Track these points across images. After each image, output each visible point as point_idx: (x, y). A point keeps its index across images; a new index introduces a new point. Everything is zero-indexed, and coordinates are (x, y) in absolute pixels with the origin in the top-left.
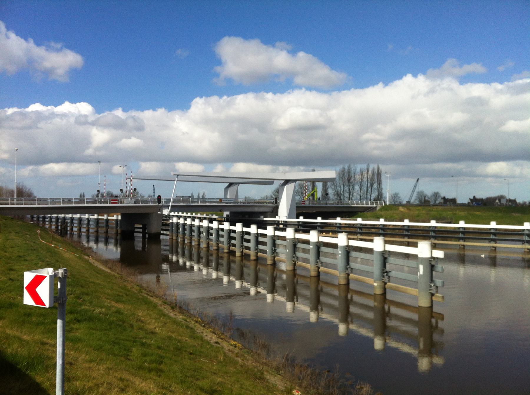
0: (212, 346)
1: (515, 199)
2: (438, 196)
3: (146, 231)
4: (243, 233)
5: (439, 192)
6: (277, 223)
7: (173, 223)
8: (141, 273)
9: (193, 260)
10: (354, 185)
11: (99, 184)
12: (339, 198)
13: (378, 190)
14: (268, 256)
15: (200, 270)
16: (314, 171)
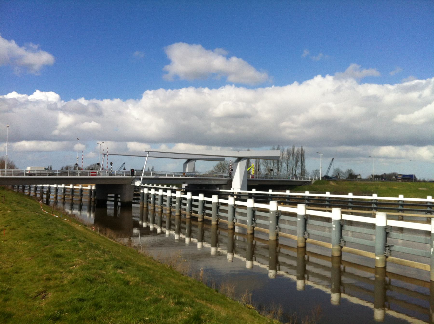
5: (353, 170)
6: (232, 195)
10: (282, 163)
11: (78, 158)
13: (302, 167)
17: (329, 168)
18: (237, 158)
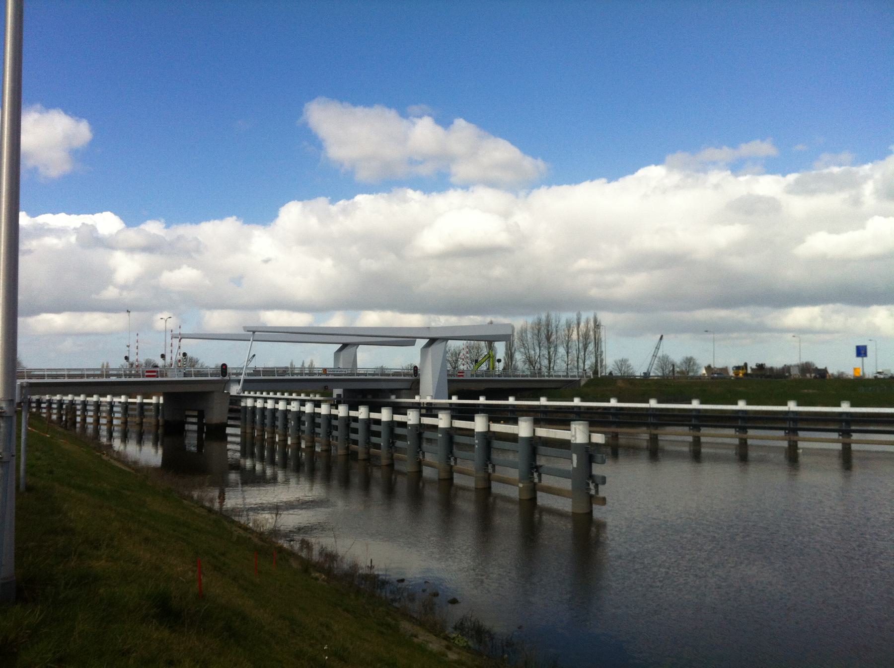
1: (826, 368)
2: (692, 363)
3: (204, 422)
5: (695, 357)
12: (532, 368)
17: (655, 355)
18: (428, 340)
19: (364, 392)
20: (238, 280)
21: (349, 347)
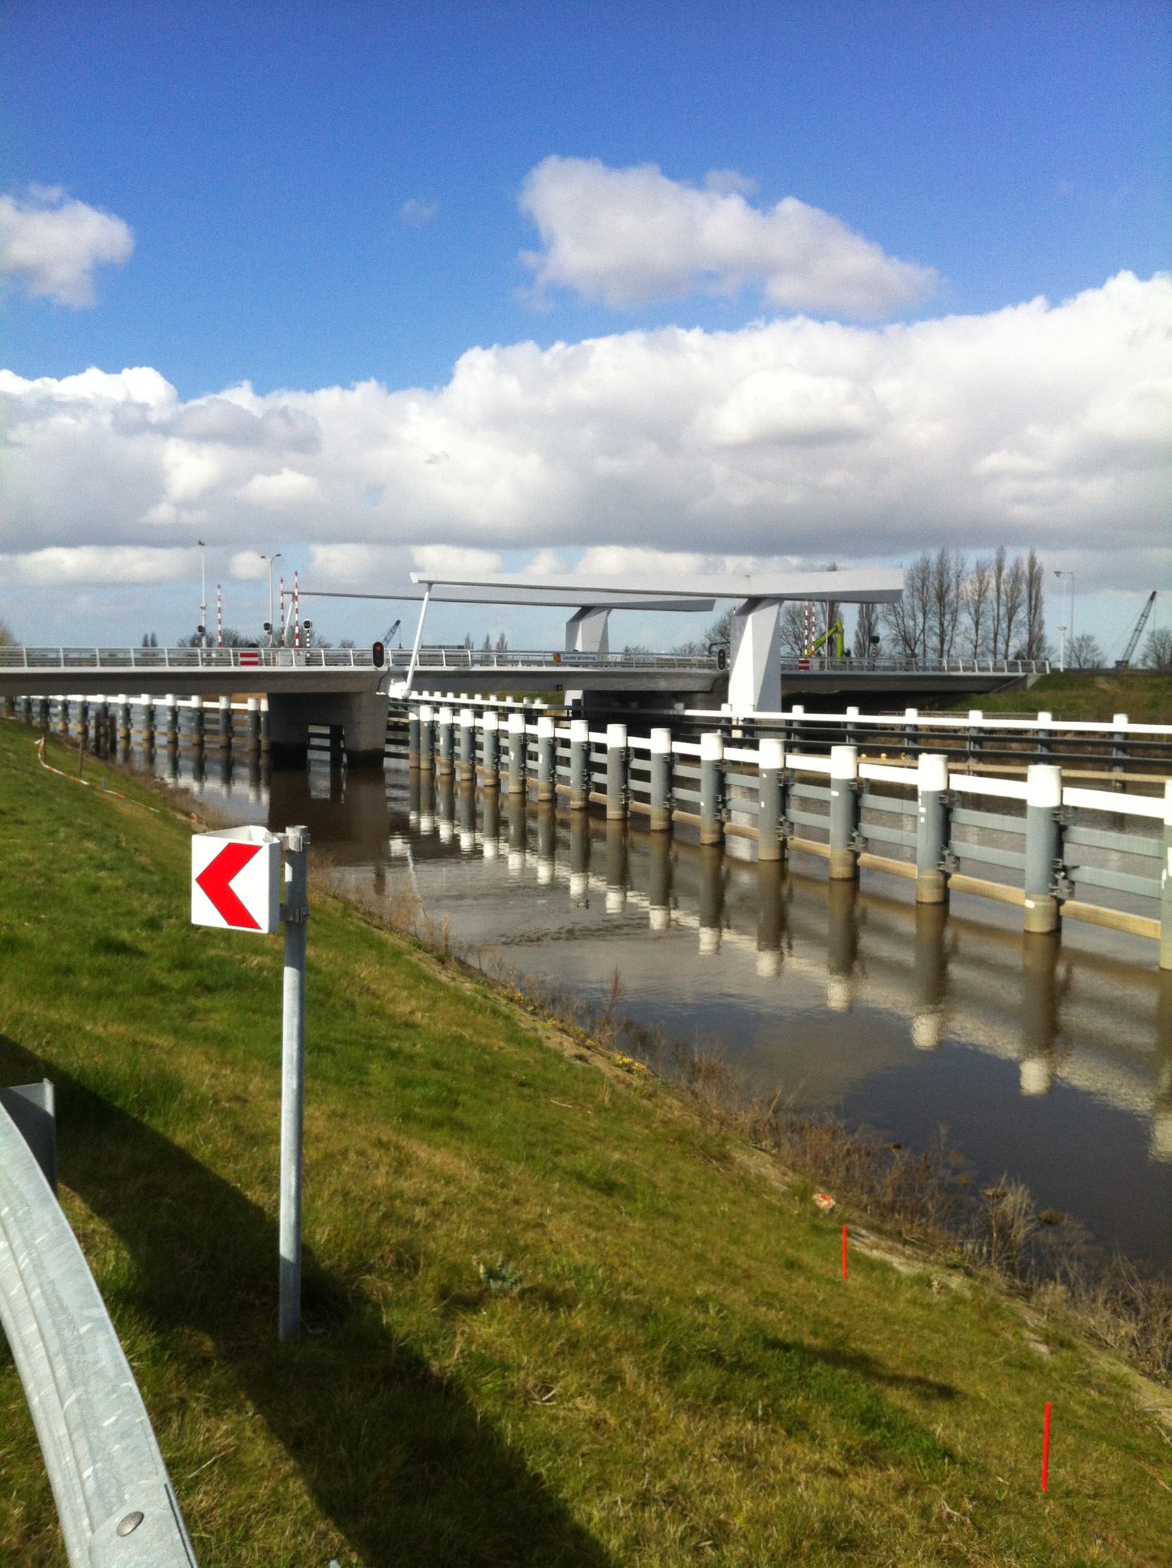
0: (571, 1067)
4: (627, 753)
6: (726, 726)
7: (418, 723)
8: (339, 862)
9: (481, 831)
10: (955, 613)
12: (909, 652)
14: (704, 820)
15: (500, 858)
16: (833, 569)
19: (624, 697)
20: (375, 491)
21: (593, 611)
